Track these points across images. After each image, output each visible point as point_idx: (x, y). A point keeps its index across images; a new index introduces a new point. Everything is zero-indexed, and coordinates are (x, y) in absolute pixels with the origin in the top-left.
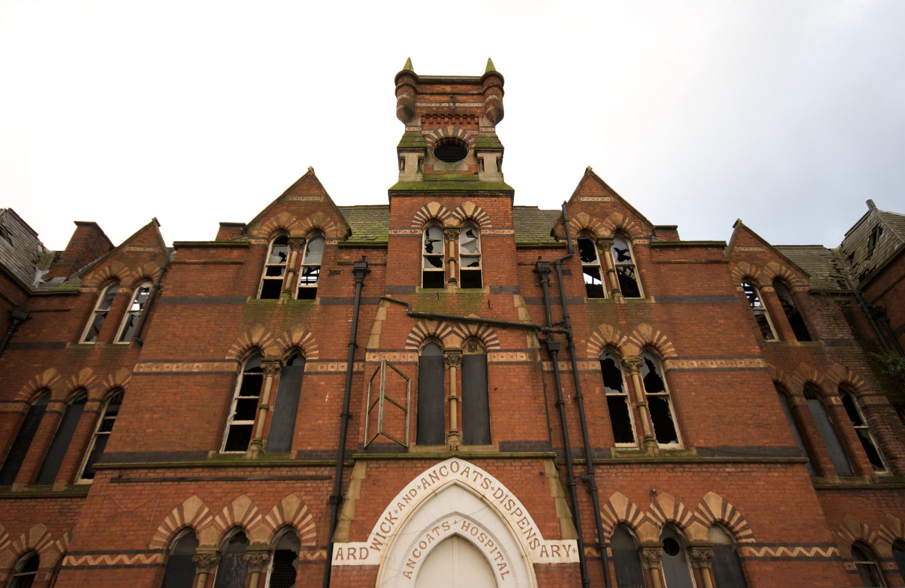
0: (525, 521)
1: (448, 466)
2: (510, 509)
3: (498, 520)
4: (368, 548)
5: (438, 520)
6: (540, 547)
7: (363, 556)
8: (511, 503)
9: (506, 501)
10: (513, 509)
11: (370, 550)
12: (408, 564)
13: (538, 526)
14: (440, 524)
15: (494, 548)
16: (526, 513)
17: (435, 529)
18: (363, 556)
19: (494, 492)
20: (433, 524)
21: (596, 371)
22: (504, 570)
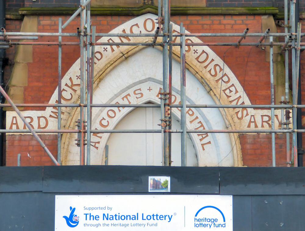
0: (232, 89)
1: (141, 24)
2: (216, 75)
3: (203, 87)
4: (47, 116)
5: (129, 88)
6: (248, 118)
7: (200, 60)
8: (218, 69)
9: (212, 66)
10: (220, 75)
11: (49, 119)
12: (104, 215)
13: (248, 95)
14: (131, 91)
15: (194, 117)
16: (234, 80)
17: (126, 97)
18: (200, 60)
19: (196, 55)
20: (123, 91)
21: (17, 165)
22: (205, 141)
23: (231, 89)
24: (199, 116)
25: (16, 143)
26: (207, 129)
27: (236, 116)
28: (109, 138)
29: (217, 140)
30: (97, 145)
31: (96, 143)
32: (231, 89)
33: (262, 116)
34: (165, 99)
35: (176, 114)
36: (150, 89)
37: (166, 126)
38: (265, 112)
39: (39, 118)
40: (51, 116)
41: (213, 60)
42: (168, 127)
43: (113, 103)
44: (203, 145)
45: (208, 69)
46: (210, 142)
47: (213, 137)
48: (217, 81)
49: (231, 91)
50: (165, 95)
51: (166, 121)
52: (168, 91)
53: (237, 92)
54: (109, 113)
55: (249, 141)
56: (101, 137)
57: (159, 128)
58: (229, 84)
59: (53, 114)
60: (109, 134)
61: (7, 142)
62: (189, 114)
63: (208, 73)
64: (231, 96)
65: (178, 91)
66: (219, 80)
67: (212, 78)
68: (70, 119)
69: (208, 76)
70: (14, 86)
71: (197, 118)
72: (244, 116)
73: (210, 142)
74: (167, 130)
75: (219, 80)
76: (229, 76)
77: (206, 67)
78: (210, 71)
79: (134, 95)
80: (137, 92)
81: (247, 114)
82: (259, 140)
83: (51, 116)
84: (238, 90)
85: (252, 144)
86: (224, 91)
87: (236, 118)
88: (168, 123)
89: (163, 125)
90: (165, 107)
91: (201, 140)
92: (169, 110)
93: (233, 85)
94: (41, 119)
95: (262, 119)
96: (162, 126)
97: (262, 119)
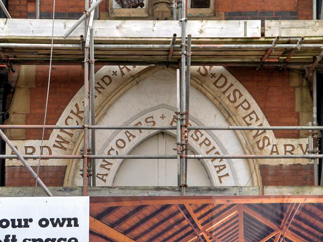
0: (253, 116)
2: (235, 101)
4: (51, 146)
6: (270, 147)
7: (218, 84)
11: (53, 149)
15: (211, 147)
16: (255, 106)
23: (251, 116)
24: (216, 146)
25: (17, 175)
26: (222, 155)
27: (256, 145)
28: (142, 143)
29: (235, 172)
30: (105, 178)
31: (103, 175)
32: (251, 116)
33: (285, 146)
34: (182, 120)
35: (192, 145)
36: (163, 117)
37: (183, 150)
38: (289, 141)
39: (42, 148)
40: (54, 146)
41: (232, 85)
42: (184, 152)
43: (132, 125)
44: (220, 177)
45: (227, 94)
46: (227, 175)
47: (231, 168)
48: (237, 108)
49: (251, 119)
50: (182, 115)
51: (182, 145)
52: (184, 111)
53: (258, 119)
54: (118, 143)
55: (270, 172)
56: (109, 169)
57: (175, 153)
58: (250, 111)
59: (57, 144)
60: (121, 160)
61: (6, 173)
62: (205, 144)
63: (283, 146)
64: (251, 124)
65: (180, 184)
66: (238, 106)
67: (231, 104)
68: (75, 149)
69: (227, 102)
70: (14, 113)
71: (214, 148)
72: (266, 145)
73: (227, 175)
74: (184, 155)
75: (238, 106)
76: (249, 101)
77: (224, 93)
78: (228, 97)
79: (145, 123)
80: (148, 120)
81: (269, 144)
82: (282, 171)
83: (54, 146)
84: (259, 117)
85: (274, 176)
86: (244, 118)
87: (257, 147)
88: (184, 147)
89: (179, 149)
90: (181, 129)
91: (218, 172)
92: (186, 132)
93: (254, 112)
94: (44, 149)
95: (285, 148)
96: (178, 151)
97: (285, 148)
